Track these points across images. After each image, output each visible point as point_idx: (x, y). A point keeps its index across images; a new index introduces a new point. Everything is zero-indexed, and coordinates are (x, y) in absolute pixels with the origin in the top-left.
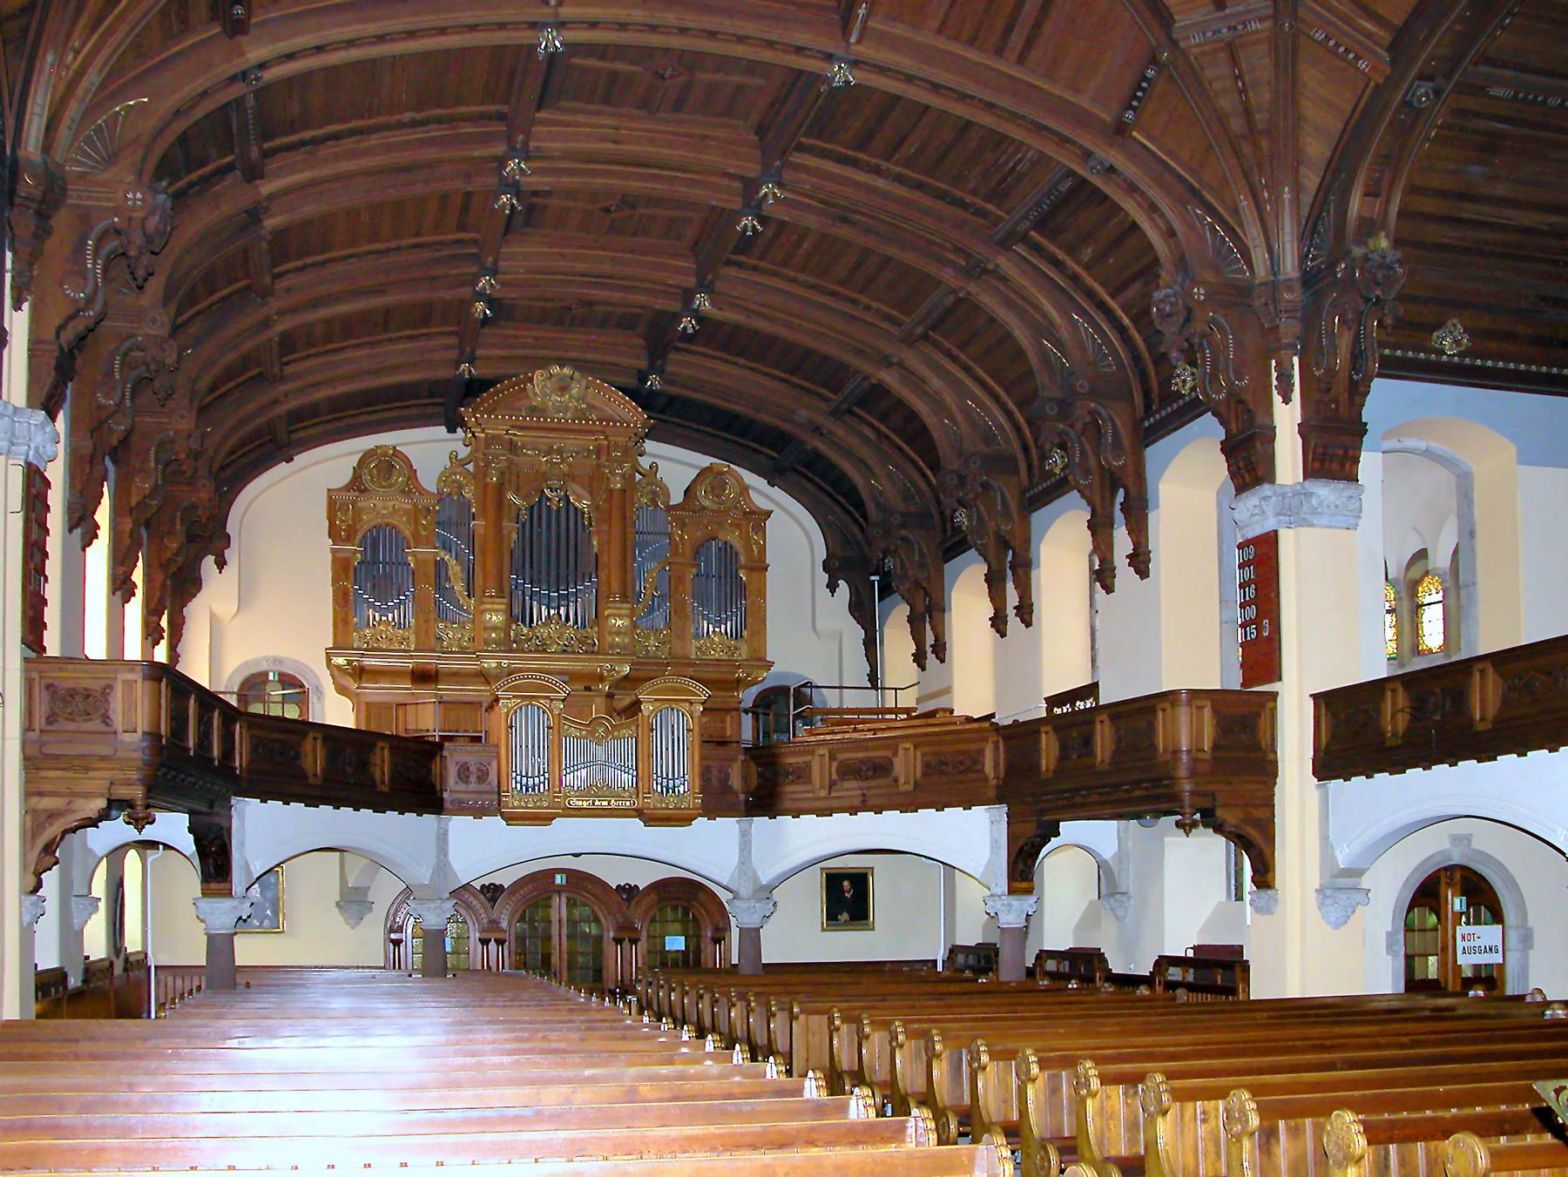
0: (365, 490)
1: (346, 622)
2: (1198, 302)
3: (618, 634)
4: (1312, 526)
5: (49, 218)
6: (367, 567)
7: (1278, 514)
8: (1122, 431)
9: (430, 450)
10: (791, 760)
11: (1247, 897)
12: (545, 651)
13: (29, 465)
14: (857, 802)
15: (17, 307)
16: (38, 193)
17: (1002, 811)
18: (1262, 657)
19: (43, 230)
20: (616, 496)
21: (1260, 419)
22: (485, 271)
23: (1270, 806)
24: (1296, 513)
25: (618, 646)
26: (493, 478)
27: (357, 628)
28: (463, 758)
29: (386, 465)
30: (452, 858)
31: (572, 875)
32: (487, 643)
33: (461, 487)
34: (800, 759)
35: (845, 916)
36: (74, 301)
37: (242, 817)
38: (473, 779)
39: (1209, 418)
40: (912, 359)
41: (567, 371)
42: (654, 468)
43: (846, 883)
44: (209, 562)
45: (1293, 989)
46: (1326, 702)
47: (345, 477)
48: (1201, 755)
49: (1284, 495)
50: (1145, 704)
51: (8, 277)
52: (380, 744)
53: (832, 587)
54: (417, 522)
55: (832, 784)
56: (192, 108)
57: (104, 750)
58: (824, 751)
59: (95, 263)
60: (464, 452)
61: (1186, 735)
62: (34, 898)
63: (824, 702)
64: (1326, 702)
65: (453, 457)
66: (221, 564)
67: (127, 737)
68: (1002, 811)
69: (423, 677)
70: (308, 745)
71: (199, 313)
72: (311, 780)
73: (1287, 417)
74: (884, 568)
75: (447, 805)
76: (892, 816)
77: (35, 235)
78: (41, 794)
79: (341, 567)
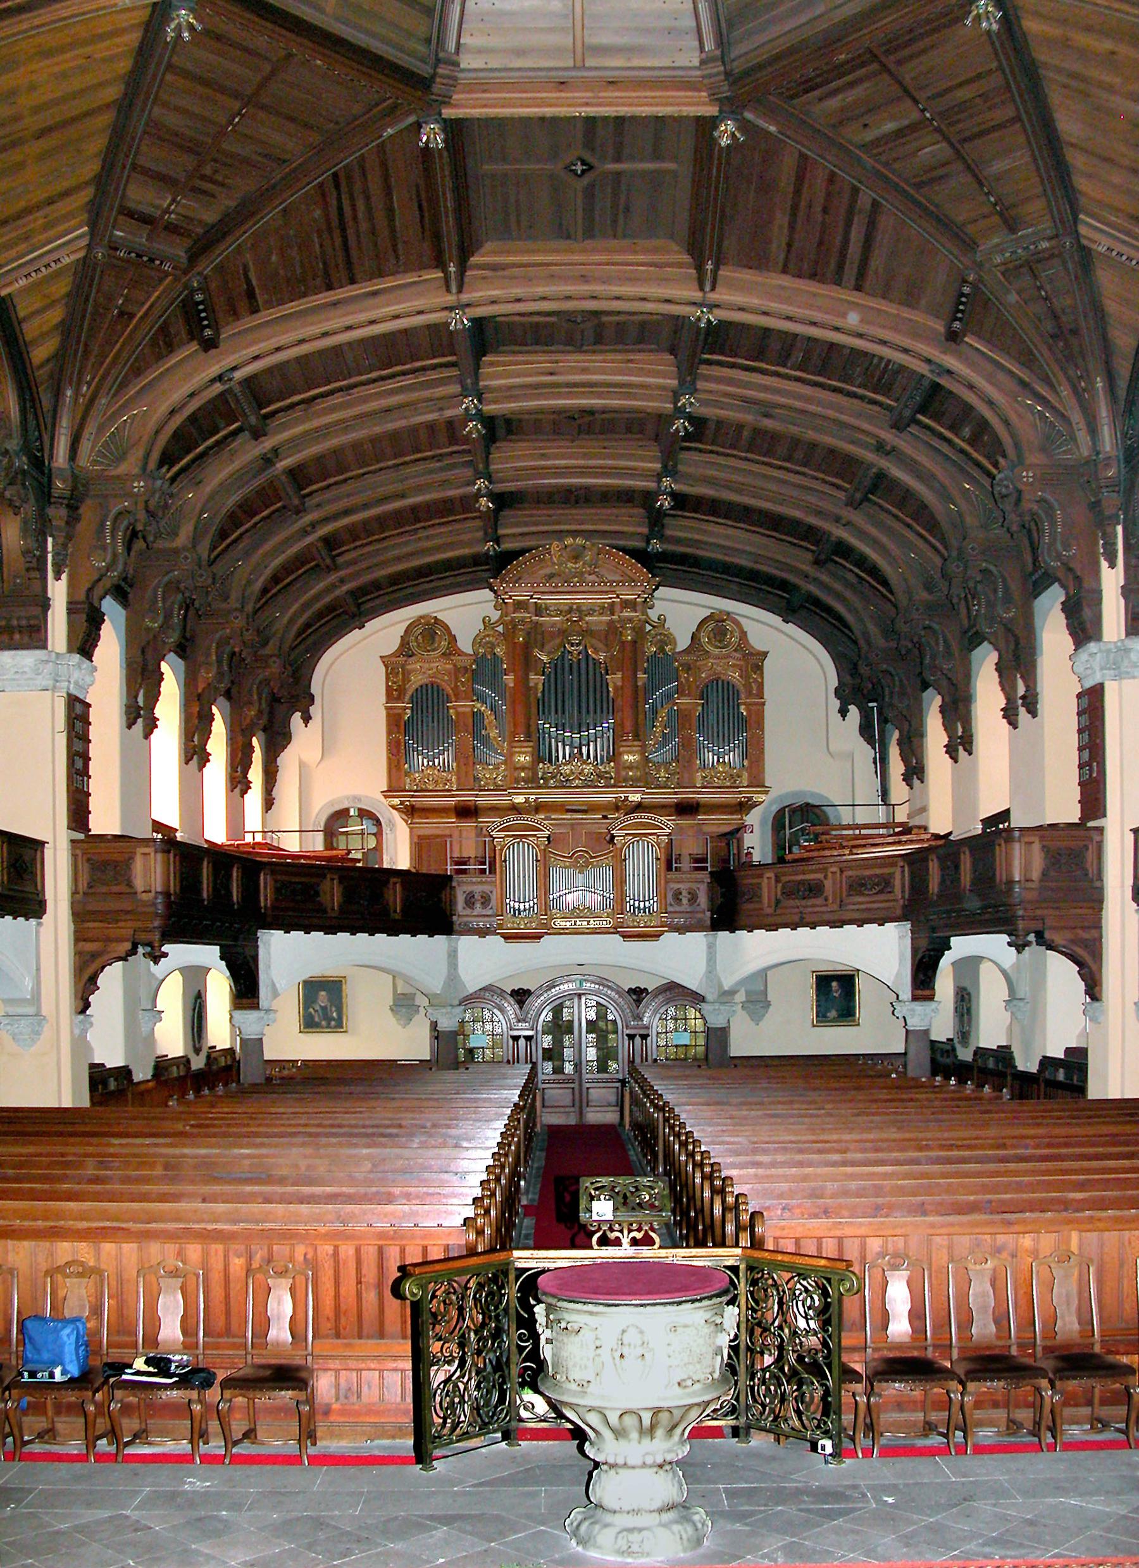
0: (413, 655)
1: (398, 767)
2: (1026, 484)
3: (630, 768)
4: (1134, 677)
5: (77, 508)
6: (417, 716)
7: (1102, 669)
8: (1013, 587)
9: (466, 613)
10: (746, 881)
13: (69, 695)
14: (796, 919)
15: (58, 578)
16: (68, 494)
17: (908, 925)
18: (1093, 797)
19: (73, 519)
20: (629, 648)
21: (1087, 583)
22: (478, 475)
23: (1097, 925)
24: (1118, 666)
25: (631, 778)
26: (520, 639)
27: (407, 774)
28: (469, 888)
29: (430, 632)
30: (461, 971)
32: (517, 781)
33: (493, 647)
36: (99, 569)
37: (268, 944)
38: (478, 905)
39: (1056, 586)
40: (857, 517)
42: (662, 619)
43: (834, 984)
44: (297, 718)
47: (394, 645)
48: (1029, 885)
49: (1108, 651)
51: (50, 556)
52: (393, 880)
53: (843, 712)
54: (457, 680)
55: (778, 902)
56: (184, 405)
58: (771, 874)
59: (113, 536)
60: (495, 615)
61: (1022, 865)
62: (81, 1017)
63: (838, 817)
65: (485, 622)
66: (307, 719)
67: (145, 897)
68: (908, 925)
69: (466, 812)
71: (247, 531)
74: (894, 687)
75: (456, 927)
77: (67, 523)
79: (394, 722)
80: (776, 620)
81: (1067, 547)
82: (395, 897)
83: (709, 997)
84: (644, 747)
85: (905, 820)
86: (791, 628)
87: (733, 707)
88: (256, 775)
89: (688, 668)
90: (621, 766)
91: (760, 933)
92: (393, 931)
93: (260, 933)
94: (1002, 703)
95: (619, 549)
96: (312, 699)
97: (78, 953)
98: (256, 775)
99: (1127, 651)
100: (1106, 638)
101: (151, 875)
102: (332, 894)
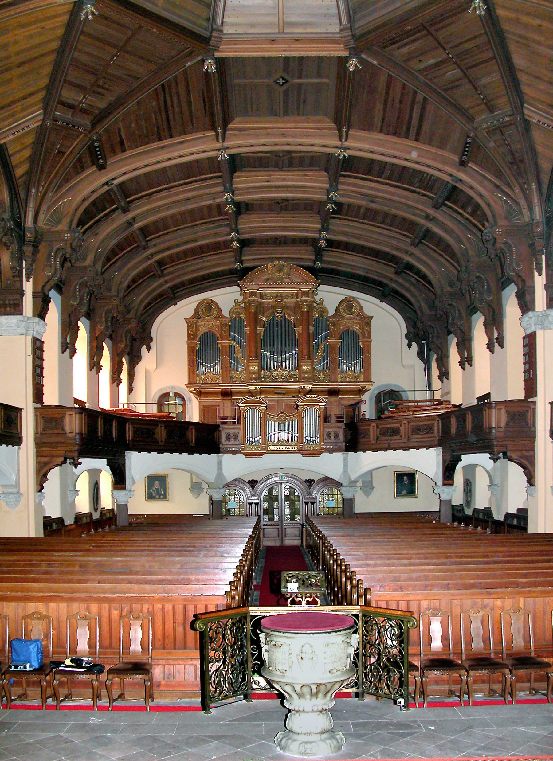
0: (201, 318)
1: (193, 372)
2: (498, 235)
3: (306, 373)
4: (551, 329)
5: (37, 247)
6: (202, 348)
7: (535, 325)
8: (492, 285)
9: (226, 298)
10: (362, 428)
13: (34, 337)
14: (387, 446)
15: (28, 280)
16: (33, 240)
17: (441, 449)
18: (531, 387)
19: (36, 252)
20: (305, 315)
21: (528, 283)
22: (232, 231)
23: (533, 449)
24: (543, 323)
25: (306, 378)
26: (253, 310)
27: (198, 376)
28: (228, 431)
29: (209, 307)
30: (224, 471)
32: (251, 379)
33: (239, 314)
36: (48, 276)
37: (130, 458)
38: (232, 439)
39: (513, 285)
40: (416, 251)
42: (321, 301)
43: (405, 478)
44: (144, 349)
45: (541, 531)
47: (191, 313)
48: (500, 429)
49: (538, 316)
51: (24, 270)
52: (191, 427)
53: (409, 346)
54: (222, 330)
55: (378, 438)
56: (89, 197)
58: (374, 424)
59: (55, 260)
60: (240, 299)
61: (496, 420)
62: (40, 494)
63: (407, 397)
65: (236, 302)
66: (149, 349)
67: (70, 435)
68: (441, 449)
69: (226, 394)
71: (120, 258)
74: (434, 333)
75: (221, 450)
77: (33, 254)
79: (191, 350)
80: (377, 301)
81: (518, 265)
82: (192, 435)
83: (344, 484)
84: (312, 363)
85: (439, 398)
86: (384, 305)
87: (356, 343)
88: (124, 376)
89: (334, 324)
90: (301, 372)
91: (369, 453)
92: (191, 452)
93: (126, 453)
94: (487, 341)
95: (301, 266)
96: (151, 339)
97: (38, 463)
98: (124, 376)
99: (547, 316)
100: (537, 310)
101: (73, 425)
102: (161, 434)
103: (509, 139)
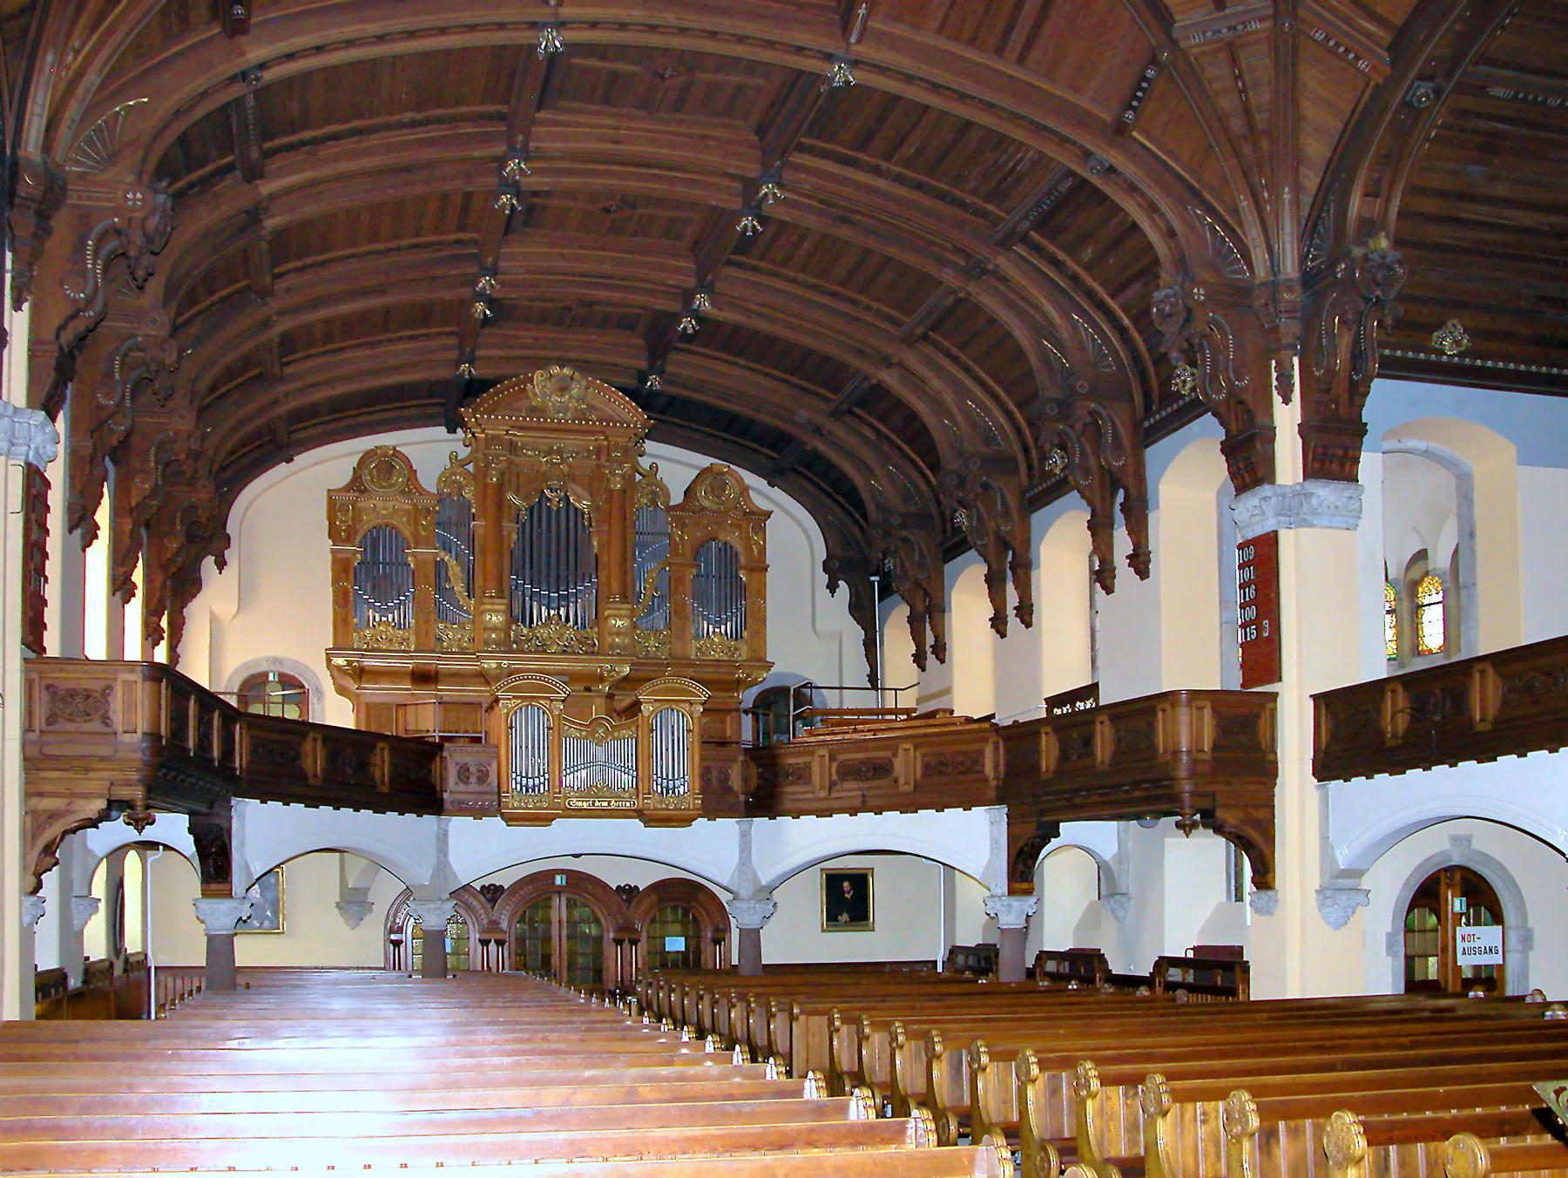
0: (365, 491)
1: (346, 622)
2: (1198, 302)
3: (618, 634)
4: (1312, 526)
5: (49, 218)
6: (367, 567)
7: (1278, 515)
8: (1122, 431)
9: (430, 450)
10: (791, 761)
11: (1247, 898)
12: (545, 652)
13: (29, 465)
14: (857, 803)
15: (17, 307)
16: (38, 193)
17: (1002, 811)
18: (1262, 658)
19: (43, 230)
20: (616, 497)
21: (1260, 420)
22: (485, 271)
23: (1270, 806)
24: (1296, 513)
25: (618, 646)
26: (493, 478)
27: (357, 629)
28: (463, 759)
29: (386, 465)
30: (452, 859)
31: (572, 875)
32: (487, 643)
33: (461, 487)
34: (800, 760)
35: (845, 917)
36: (74, 301)
37: (242, 818)
38: (473, 780)
39: (1209, 418)
40: (912, 359)
41: (567, 371)
42: (654, 468)
43: (846, 884)
44: (209, 562)
46: (1326, 702)
47: (345, 477)
48: (1201, 756)
49: (1284, 496)
50: (1145, 704)
51: (8, 277)
52: (380, 745)
53: (832, 587)
54: (417, 523)
55: (832, 784)
56: (192, 108)
57: (104, 751)
58: (824, 752)
59: (95, 264)
60: (464, 453)
61: (1186, 735)
62: (34, 899)
63: (824, 702)
64: (1326, 702)
65: (453, 457)
66: (221, 564)
67: (127, 738)
68: (1002, 811)
69: (423, 677)
70: (308, 745)
71: (199, 313)
72: (311, 781)
73: (1287, 418)
74: (884, 569)
75: (447, 806)
76: (892, 816)
77: (35, 235)
78: (41, 795)
79: (341, 568)
86: (301, 459)
103: (1247, 78)
